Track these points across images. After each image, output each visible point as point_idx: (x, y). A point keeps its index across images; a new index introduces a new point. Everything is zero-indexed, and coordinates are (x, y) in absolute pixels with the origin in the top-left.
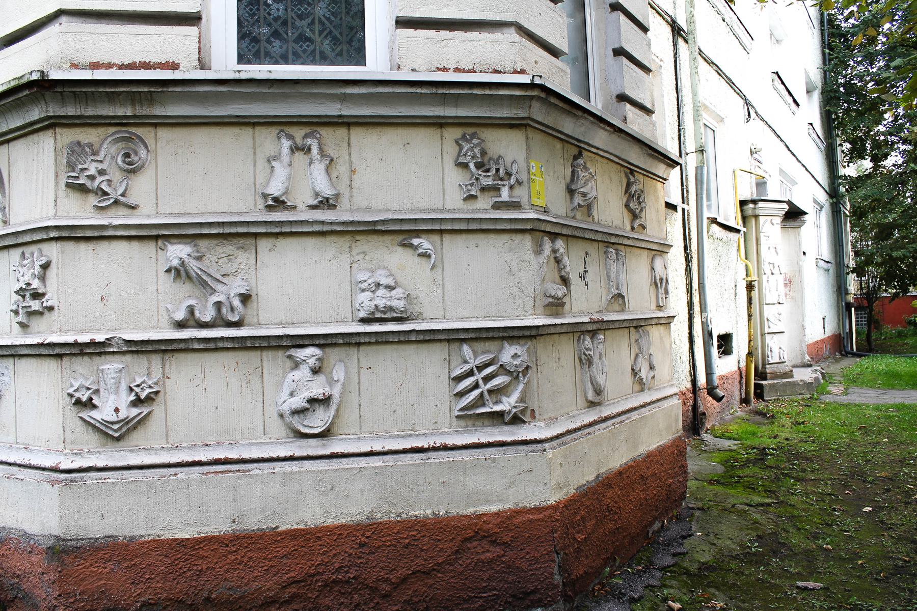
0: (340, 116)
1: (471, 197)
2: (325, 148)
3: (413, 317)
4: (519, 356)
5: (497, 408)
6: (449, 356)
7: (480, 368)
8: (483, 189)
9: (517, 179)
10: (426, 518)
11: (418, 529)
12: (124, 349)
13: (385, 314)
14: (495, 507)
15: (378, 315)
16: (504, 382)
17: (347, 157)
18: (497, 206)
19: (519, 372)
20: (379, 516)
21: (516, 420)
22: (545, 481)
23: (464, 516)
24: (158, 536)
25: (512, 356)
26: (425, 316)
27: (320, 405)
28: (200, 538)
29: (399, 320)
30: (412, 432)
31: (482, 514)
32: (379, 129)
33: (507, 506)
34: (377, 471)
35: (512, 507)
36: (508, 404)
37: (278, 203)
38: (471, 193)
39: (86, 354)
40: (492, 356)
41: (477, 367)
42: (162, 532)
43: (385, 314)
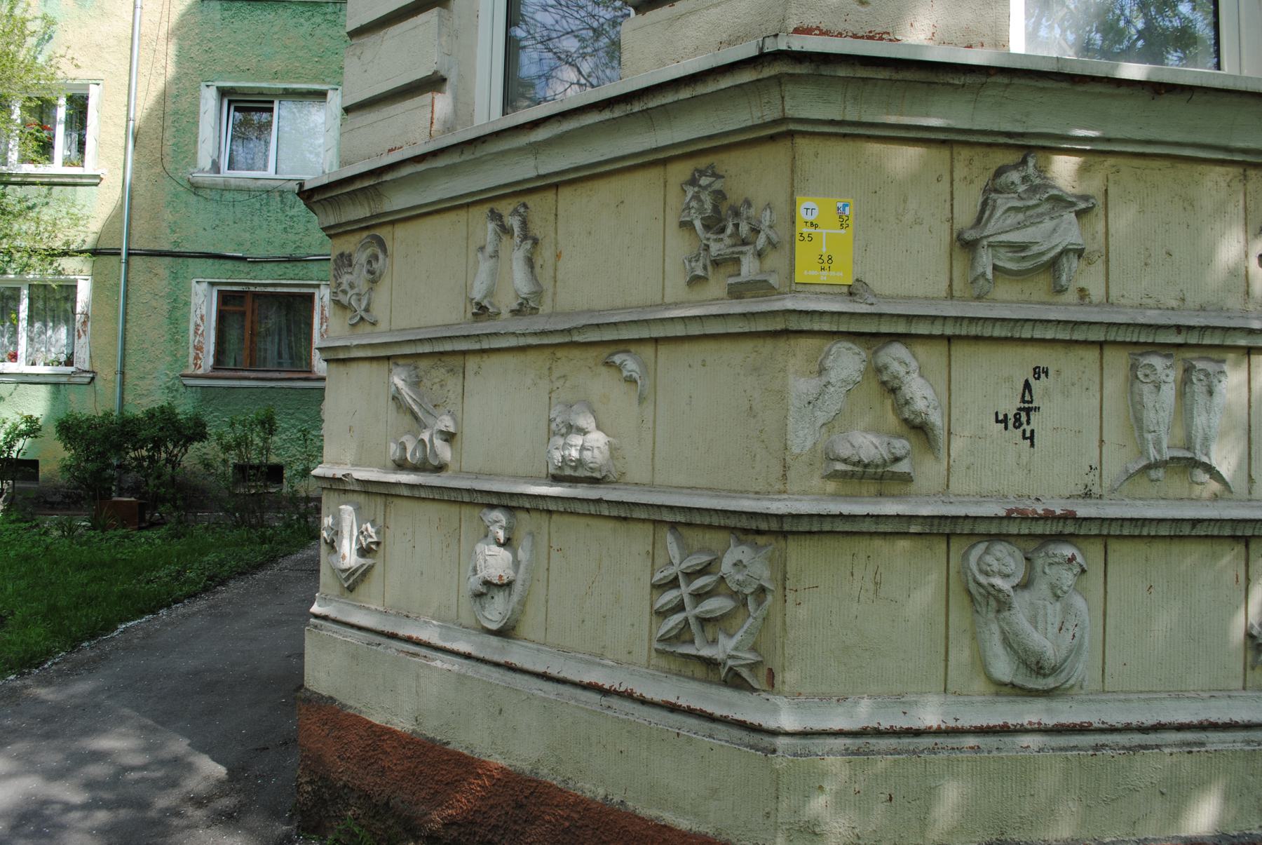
0: (539, 177)
1: (695, 281)
2: (531, 226)
3: (612, 478)
4: (745, 566)
5: (706, 652)
6: (654, 548)
7: (691, 575)
8: (717, 263)
9: (768, 237)
10: (593, 800)
11: (579, 812)
12: (357, 489)
13: (575, 471)
14: (687, 823)
15: (568, 472)
16: (720, 608)
17: (553, 235)
18: (736, 292)
19: (747, 595)
20: (545, 773)
21: (735, 681)
22: (767, 810)
23: (640, 818)
24: (360, 712)
25: (735, 565)
26: (628, 478)
27: (499, 591)
28: (385, 728)
29: (593, 481)
30: (598, 660)
31: (665, 826)
32: (589, 185)
33: (703, 829)
34: (545, 704)
35: (711, 834)
36: (724, 648)
37: (482, 311)
38: (696, 273)
39: (335, 490)
40: (705, 559)
41: (687, 574)
42: (364, 709)
43: (575, 471)
